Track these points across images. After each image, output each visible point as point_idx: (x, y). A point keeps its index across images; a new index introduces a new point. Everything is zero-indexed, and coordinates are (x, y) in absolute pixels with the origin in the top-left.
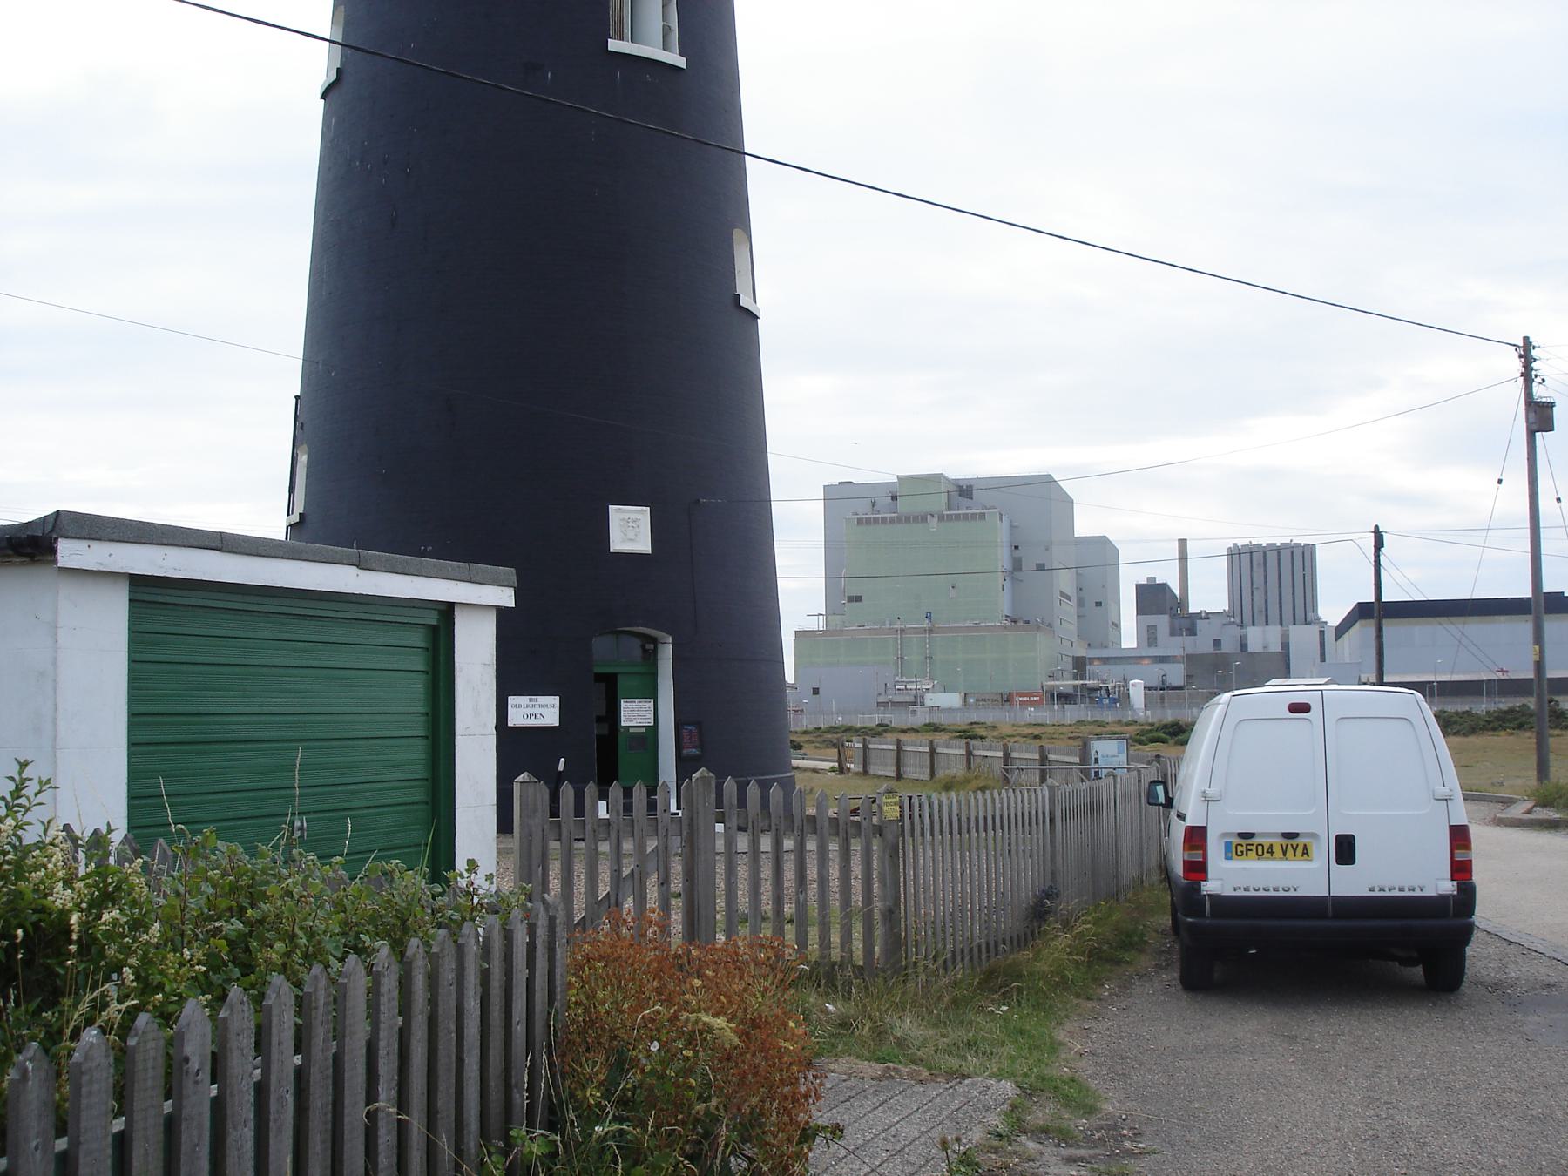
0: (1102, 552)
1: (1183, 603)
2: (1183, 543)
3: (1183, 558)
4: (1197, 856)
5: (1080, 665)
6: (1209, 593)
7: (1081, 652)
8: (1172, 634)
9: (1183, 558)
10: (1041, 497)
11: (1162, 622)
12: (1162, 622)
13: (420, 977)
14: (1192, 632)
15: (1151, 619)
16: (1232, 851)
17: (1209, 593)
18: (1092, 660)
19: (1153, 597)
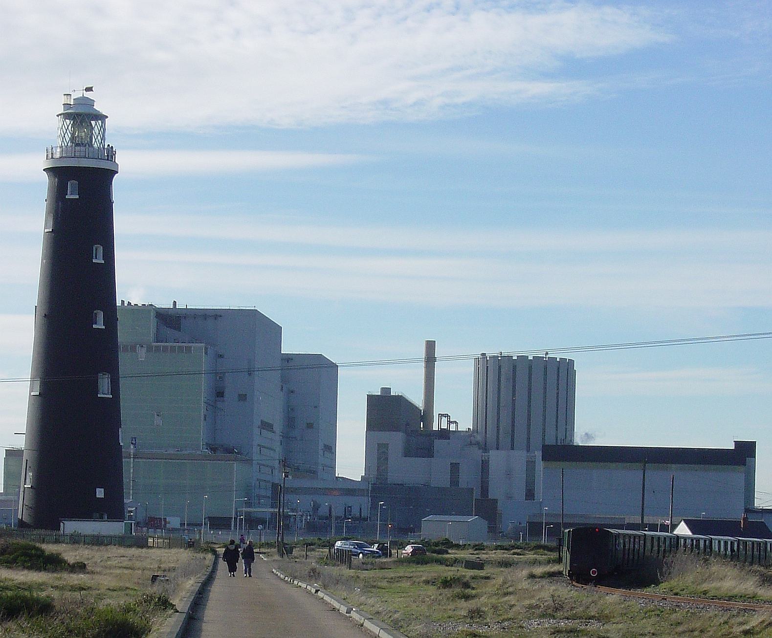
0: (319, 373)
1: (426, 415)
2: (430, 346)
3: (430, 360)
4: (67, 539)
5: (277, 492)
6: (457, 406)
7: (279, 476)
8: (407, 453)
9: (430, 360)
10: (248, 330)
11: (396, 440)
12: (396, 440)
13: (729, 549)
14: (428, 452)
15: (385, 436)
16: (560, 573)
17: (457, 406)
18: (295, 491)
19: (386, 411)
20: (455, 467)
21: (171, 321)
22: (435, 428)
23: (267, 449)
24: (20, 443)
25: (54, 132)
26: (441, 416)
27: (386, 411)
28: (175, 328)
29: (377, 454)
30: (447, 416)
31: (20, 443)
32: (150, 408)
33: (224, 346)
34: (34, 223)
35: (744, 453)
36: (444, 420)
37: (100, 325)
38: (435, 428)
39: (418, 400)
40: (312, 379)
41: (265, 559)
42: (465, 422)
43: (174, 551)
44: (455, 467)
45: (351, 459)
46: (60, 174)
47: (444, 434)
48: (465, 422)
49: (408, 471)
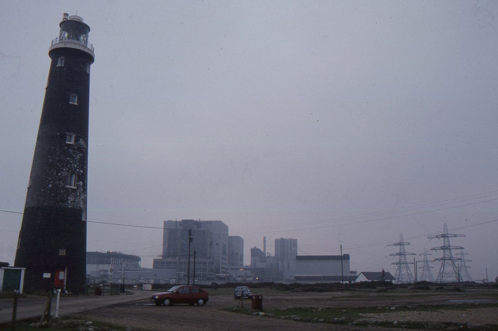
0: (238, 240)
1: (264, 253)
3: (486, 269)
6: (271, 251)
9: (486, 269)
17: (271, 251)
19: (255, 252)
22: (266, 256)
25: (52, 35)
26: (268, 253)
27: (255, 252)
28: (357, 277)
29: (253, 261)
30: (269, 253)
36: (268, 254)
37: (75, 102)
38: (266, 256)
39: (262, 250)
42: (273, 254)
45: (247, 261)
47: (268, 257)
48: (273, 254)
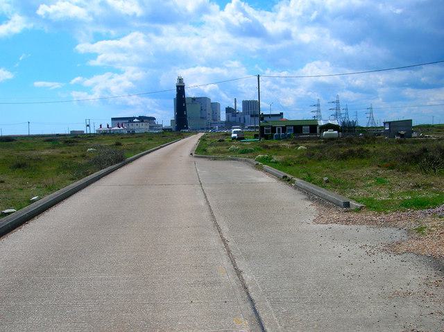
1: (235, 110)
6: (240, 108)
11: (230, 114)
12: (230, 114)
17: (240, 108)
19: (228, 110)
20: (240, 119)
21: (194, 99)
23: (210, 119)
24: (174, 119)
25: (176, 82)
29: (228, 117)
31: (174, 119)
32: (190, 111)
33: (201, 101)
34: (175, 92)
35: (282, 114)
40: (215, 106)
41: (308, 112)
43: (99, 42)
44: (240, 119)
46: (178, 87)
49: (232, 119)
